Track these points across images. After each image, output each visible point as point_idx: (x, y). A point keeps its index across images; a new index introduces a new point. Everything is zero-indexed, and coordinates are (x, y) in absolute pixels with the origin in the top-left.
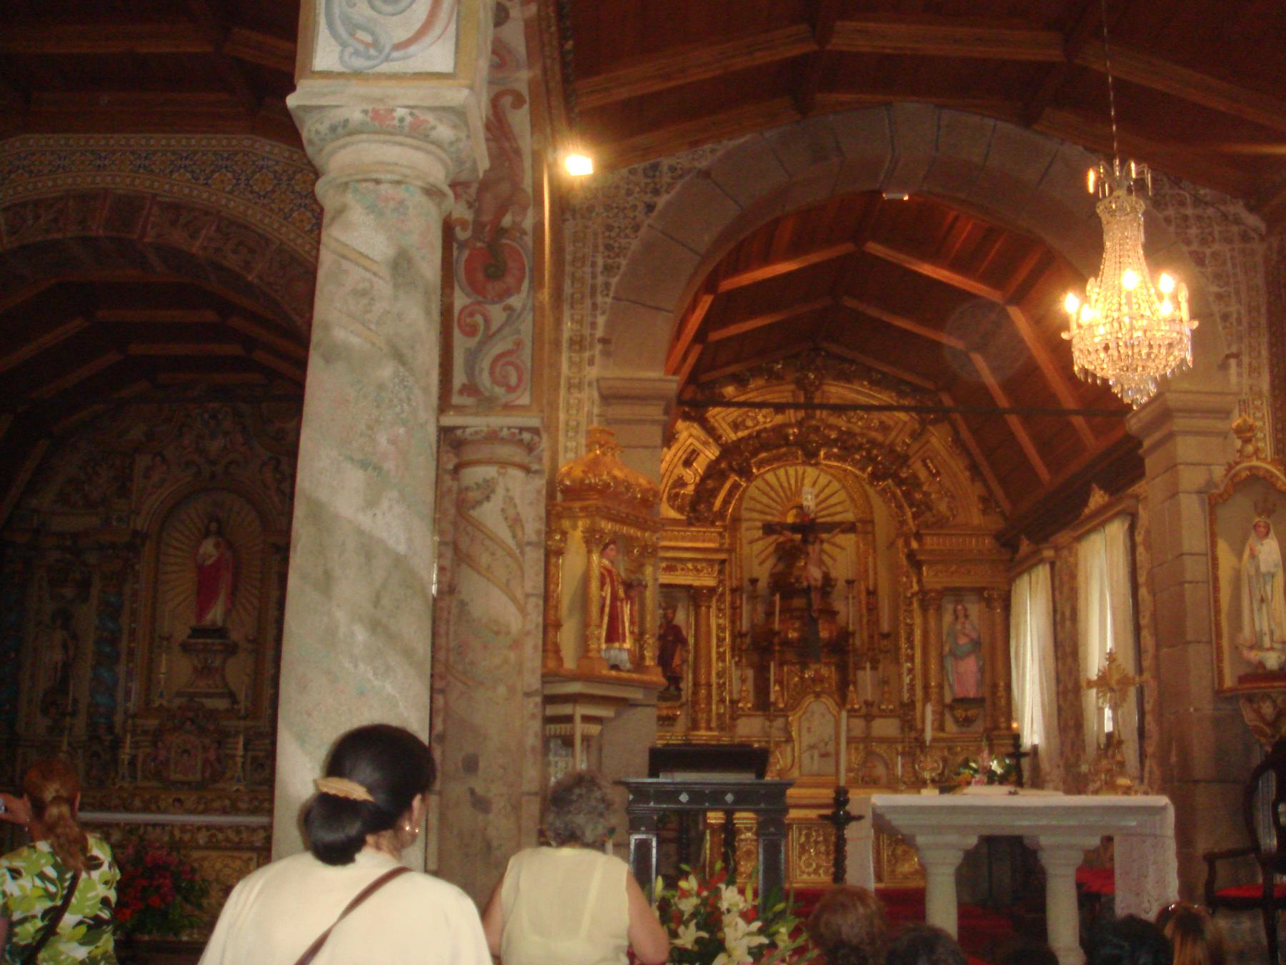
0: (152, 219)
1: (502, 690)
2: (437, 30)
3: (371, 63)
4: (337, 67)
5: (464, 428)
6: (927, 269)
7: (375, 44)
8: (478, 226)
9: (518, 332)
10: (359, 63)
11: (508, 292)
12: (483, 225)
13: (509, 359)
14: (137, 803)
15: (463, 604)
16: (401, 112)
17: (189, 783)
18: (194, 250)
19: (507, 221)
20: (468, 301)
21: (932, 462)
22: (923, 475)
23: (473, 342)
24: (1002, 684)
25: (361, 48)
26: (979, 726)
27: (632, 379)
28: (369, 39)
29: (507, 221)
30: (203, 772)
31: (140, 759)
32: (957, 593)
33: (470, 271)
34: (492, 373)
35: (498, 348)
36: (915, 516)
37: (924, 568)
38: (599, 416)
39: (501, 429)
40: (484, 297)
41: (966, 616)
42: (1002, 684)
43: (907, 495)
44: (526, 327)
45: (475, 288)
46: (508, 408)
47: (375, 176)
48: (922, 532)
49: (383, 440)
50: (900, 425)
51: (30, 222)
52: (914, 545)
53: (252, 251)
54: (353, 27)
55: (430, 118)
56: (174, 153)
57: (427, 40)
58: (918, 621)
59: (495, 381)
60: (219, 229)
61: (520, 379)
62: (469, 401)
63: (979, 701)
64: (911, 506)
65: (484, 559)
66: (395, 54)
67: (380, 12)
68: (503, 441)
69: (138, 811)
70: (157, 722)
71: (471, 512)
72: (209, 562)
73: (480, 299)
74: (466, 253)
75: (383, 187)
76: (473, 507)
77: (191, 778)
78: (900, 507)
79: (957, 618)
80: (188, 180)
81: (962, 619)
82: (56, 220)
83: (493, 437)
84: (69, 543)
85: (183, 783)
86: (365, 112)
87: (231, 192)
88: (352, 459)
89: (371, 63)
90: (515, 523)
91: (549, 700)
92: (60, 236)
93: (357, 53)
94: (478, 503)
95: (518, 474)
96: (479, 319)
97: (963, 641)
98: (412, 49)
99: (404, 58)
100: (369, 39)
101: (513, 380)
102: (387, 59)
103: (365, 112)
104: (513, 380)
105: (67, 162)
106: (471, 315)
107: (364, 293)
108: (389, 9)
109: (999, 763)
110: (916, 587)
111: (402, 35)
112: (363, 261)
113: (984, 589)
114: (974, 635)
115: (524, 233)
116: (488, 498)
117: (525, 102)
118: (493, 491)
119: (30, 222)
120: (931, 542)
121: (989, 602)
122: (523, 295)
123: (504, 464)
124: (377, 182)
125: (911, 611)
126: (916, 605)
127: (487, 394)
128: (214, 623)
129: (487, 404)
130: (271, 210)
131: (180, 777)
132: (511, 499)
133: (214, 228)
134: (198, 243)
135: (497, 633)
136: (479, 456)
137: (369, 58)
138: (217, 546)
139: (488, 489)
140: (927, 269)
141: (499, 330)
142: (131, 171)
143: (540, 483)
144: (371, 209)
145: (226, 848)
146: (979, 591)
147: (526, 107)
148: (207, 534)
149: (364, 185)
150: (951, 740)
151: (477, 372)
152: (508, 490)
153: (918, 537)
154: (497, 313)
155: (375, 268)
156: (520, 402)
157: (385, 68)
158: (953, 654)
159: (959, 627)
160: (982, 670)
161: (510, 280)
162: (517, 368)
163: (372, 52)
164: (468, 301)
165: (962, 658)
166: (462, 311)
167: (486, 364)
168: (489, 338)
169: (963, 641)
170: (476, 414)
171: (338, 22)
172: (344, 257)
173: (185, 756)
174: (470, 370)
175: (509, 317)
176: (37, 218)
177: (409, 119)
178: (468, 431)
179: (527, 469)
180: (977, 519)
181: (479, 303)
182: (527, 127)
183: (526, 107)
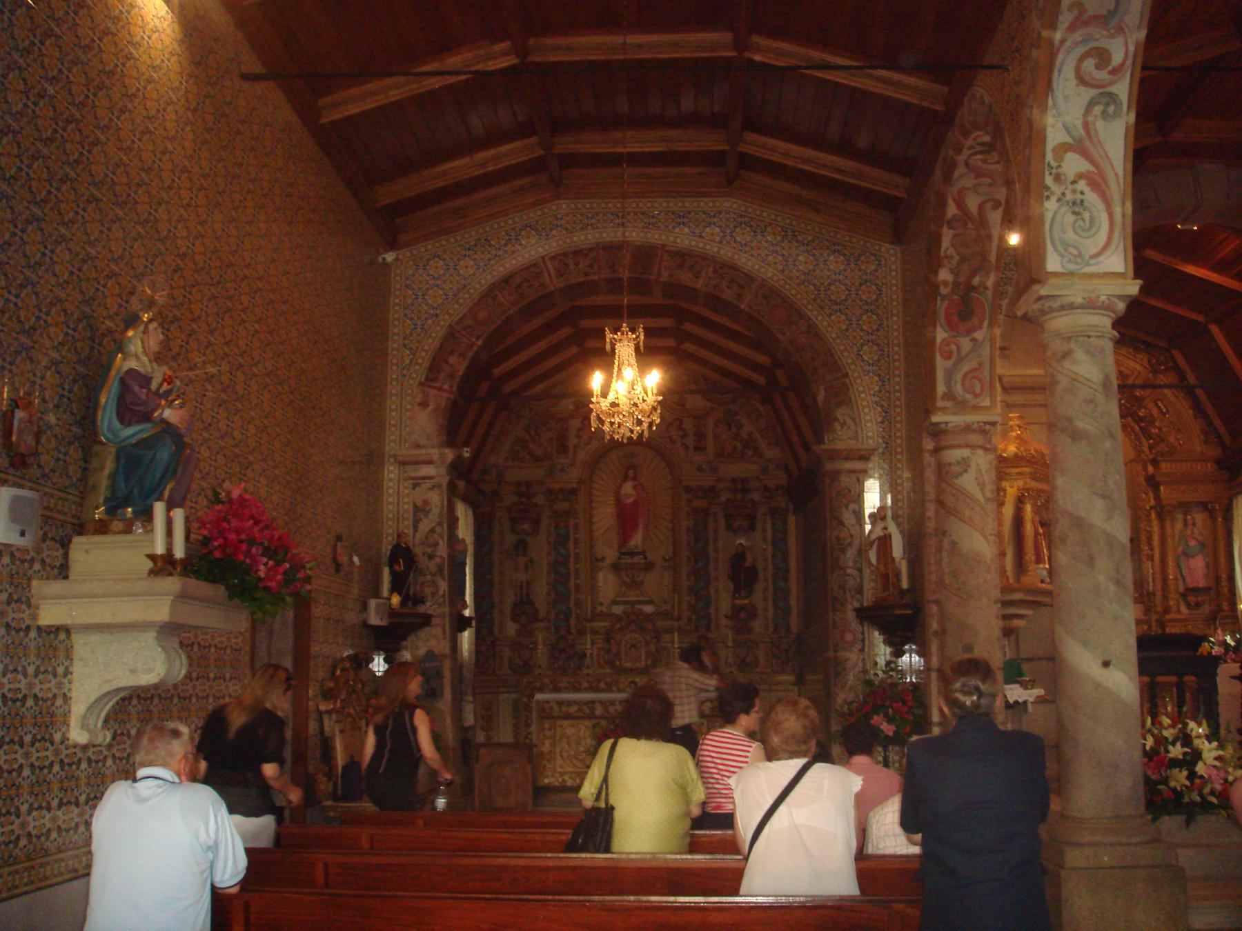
0: (664, 264)
1: (985, 600)
2: (1113, 247)
3: (1078, 267)
4: (1060, 270)
5: (947, 423)
6: (1191, 270)
7: (1080, 255)
8: (956, 285)
9: (981, 356)
10: (1072, 267)
11: (974, 329)
12: (960, 284)
13: (976, 374)
14: (602, 685)
15: (954, 544)
16: (1103, 298)
17: (636, 669)
18: (699, 286)
19: (976, 281)
20: (945, 335)
21: (1163, 403)
22: (1155, 412)
23: (949, 363)
24: (1224, 576)
25: (1072, 258)
26: (1206, 609)
27: (1024, 376)
28: (1075, 252)
29: (976, 281)
30: (646, 660)
31: (595, 654)
32: (1185, 507)
33: (947, 314)
34: (963, 384)
35: (966, 367)
36: (1151, 448)
37: (1162, 488)
38: (1002, 401)
39: (973, 423)
40: (958, 332)
41: (1194, 524)
42: (1224, 576)
43: (1145, 431)
44: (985, 352)
45: (951, 326)
46: (976, 408)
47: (1089, 334)
48: (1159, 458)
49: (1111, 483)
50: (1136, 373)
51: (572, 267)
52: (1151, 469)
53: (742, 287)
54: (1067, 245)
55: (1117, 301)
56: (673, 213)
57: (1109, 252)
58: (1156, 529)
59: (965, 390)
60: (715, 271)
61: (982, 389)
62: (949, 404)
63: (1207, 590)
64: (1148, 440)
65: (967, 513)
66: (1092, 262)
67: (1080, 236)
68: (974, 431)
69: (603, 691)
70: (607, 624)
71: (954, 480)
72: (630, 500)
73: (955, 334)
74: (946, 303)
75: (1092, 340)
76: (957, 477)
77: (638, 665)
78: (1137, 439)
79: (1186, 525)
80: (687, 234)
81: (1190, 527)
82: (591, 266)
83: (968, 429)
84: (523, 489)
85: (631, 670)
86: (1084, 298)
87: (720, 242)
88: (1097, 494)
89: (1078, 267)
90: (982, 487)
91: (1006, 604)
92: (596, 277)
93: (1070, 261)
94: (960, 474)
95: (980, 452)
96: (953, 347)
97: (1192, 543)
98: (1101, 259)
99: (1096, 264)
100: (1075, 252)
101: (978, 390)
102: (1087, 265)
103: (1084, 298)
104: (978, 390)
105: (593, 221)
106: (948, 345)
107: (1091, 401)
108: (1086, 234)
109: (1231, 637)
110: (1153, 502)
111: (1094, 251)
112: (1090, 384)
113: (1208, 503)
114: (1201, 538)
115: (987, 288)
116: (966, 471)
117: (1001, 205)
118: (969, 466)
119: (572, 267)
120: (1165, 467)
121: (1211, 514)
122: (984, 330)
123: (973, 447)
124: (1089, 337)
125: (1150, 521)
126: (1153, 516)
127: (960, 399)
128: (637, 547)
129: (962, 406)
130: (752, 255)
131: (628, 665)
132: (980, 470)
133: (711, 270)
134: (701, 281)
135: (979, 562)
136: (956, 442)
137: (1077, 264)
138: (634, 487)
139: (965, 464)
140: (1191, 270)
141: (967, 355)
142: (643, 227)
143: (991, 457)
144: (1088, 352)
145: (578, 718)
146: (1204, 506)
147: (1001, 209)
148: (625, 479)
149: (1081, 338)
150: (1185, 620)
151: (953, 383)
152: (978, 465)
153: (1155, 462)
154: (966, 343)
155: (1095, 387)
156: (983, 404)
157: (1087, 270)
158: (1185, 554)
159: (1189, 532)
160: (1207, 566)
161: (975, 321)
162: (980, 380)
163: (1079, 260)
164: (945, 335)
165: (1193, 557)
166: (941, 343)
167: (959, 377)
168: (960, 360)
169: (1192, 543)
170: (955, 414)
171: (1057, 243)
172: (1074, 380)
173: (633, 649)
174: (948, 382)
175: (975, 345)
176: (577, 264)
177: (1107, 302)
178: (950, 425)
179: (986, 449)
180: (1197, 446)
181: (954, 337)
182: (999, 222)
183: (1001, 209)
